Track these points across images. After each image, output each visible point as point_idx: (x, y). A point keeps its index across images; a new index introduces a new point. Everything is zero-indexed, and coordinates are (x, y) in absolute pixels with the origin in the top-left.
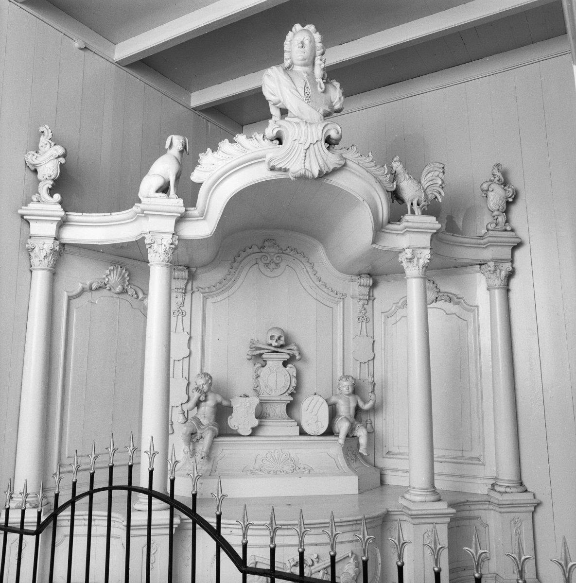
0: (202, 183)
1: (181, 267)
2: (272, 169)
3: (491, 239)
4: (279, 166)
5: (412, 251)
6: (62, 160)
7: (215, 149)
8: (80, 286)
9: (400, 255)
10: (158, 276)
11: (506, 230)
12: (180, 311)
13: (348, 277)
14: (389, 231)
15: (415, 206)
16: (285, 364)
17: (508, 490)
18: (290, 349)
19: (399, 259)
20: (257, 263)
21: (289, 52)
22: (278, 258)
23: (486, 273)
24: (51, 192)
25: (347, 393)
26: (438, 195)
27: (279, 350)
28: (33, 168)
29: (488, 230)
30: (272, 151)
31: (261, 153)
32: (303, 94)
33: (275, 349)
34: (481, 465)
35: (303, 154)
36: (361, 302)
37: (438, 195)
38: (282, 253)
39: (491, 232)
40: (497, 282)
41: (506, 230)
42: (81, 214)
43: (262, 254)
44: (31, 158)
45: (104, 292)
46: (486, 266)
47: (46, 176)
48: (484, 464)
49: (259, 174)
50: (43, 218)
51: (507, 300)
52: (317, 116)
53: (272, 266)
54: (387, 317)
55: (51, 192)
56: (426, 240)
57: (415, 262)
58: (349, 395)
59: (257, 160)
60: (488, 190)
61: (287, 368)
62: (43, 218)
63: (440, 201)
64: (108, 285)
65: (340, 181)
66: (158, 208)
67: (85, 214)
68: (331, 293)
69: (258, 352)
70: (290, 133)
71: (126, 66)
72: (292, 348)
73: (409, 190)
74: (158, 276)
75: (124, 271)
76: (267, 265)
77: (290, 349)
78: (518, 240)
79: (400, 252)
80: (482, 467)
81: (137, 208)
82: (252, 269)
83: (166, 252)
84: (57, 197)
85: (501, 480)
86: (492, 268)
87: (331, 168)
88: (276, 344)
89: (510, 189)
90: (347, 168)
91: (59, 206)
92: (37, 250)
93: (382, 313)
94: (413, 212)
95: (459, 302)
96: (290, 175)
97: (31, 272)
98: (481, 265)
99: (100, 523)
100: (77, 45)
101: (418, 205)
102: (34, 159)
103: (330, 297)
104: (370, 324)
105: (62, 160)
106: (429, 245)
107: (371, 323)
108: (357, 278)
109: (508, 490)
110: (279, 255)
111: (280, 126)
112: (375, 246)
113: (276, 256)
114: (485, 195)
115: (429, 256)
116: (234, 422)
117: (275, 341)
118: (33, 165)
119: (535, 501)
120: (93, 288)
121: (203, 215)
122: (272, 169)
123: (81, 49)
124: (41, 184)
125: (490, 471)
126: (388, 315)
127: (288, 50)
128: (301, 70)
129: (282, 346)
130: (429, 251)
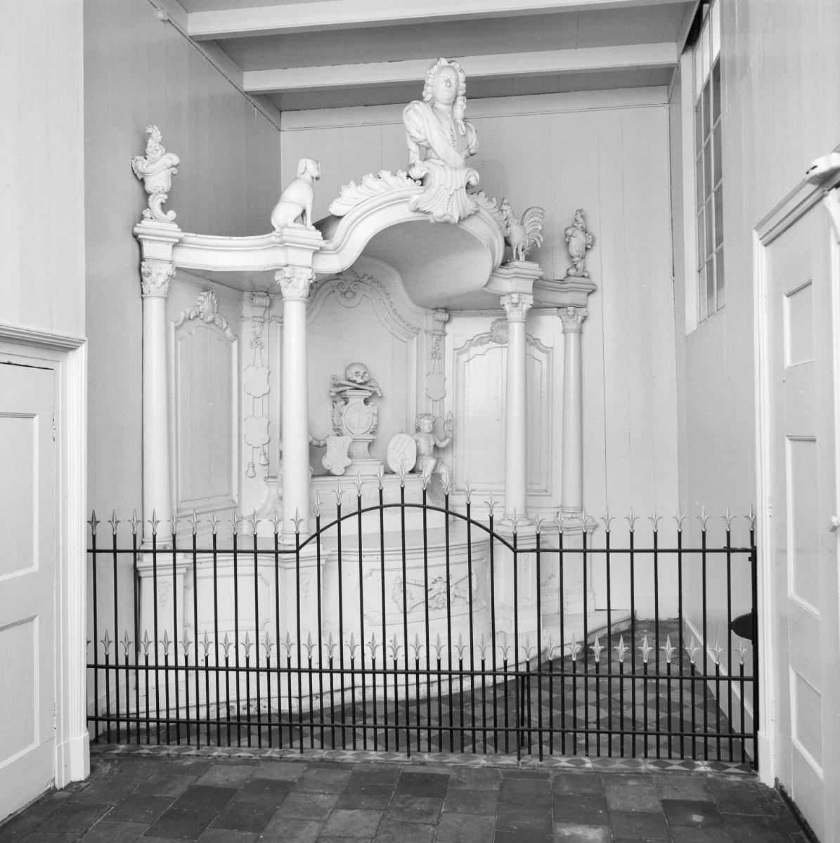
0: (340, 217)
1: (261, 294)
2: (417, 210)
3: (573, 285)
4: (424, 209)
5: (519, 296)
6: (175, 171)
7: (359, 183)
8: (182, 314)
9: (502, 298)
10: (294, 311)
11: (583, 276)
12: (258, 343)
13: (423, 311)
14: (498, 275)
15: (520, 252)
16: (366, 402)
17: (574, 516)
18: (371, 386)
19: (501, 302)
20: (334, 292)
21: (432, 86)
22: (355, 287)
23: (564, 318)
24: (165, 207)
25: (428, 431)
26: (537, 240)
27: (361, 387)
28: (140, 177)
29: (568, 275)
30: (416, 194)
31: (406, 193)
32: (449, 137)
33: (358, 386)
34: (547, 495)
35: (447, 200)
36: (435, 338)
37: (537, 240)
38: (360, 281)
39: (573, 278)
40: (573, 325)
41: (583, 276)
42: (195, 235)
43: (339, 281)
44: (142, 165)
45: (198, 322)
46: (565, 309)
47: (160, 189)
48: (550, 496)
49: (401, 214)
50: (159, 239)
51: (580, 340)
52: (460, 160)
53: (349, 295)
54: (459, 354)
55: (165, 207)
56: (528, 286)
57: (520, 308)
58: (429, 433)
59: (403, 200)
60: (572, 236)
61: (369, 406)
62: (159, 239)
63: (539, 246)
64: (202, 314)
65: (469, 226)
66: (300, 240)
67: (199, 235)
68: (406, 327)
69: (341, 389)
70: (437, 177)
71: (199, 42)
72: (373, 384)
73: (517, 239)
74: (294, 311)
75: (214, 297)
76: (344, 294)
77: (371, 386)
78: (593, 287)
79: (503, 295)
80: (549, 497)
81: (272, 237)
82: (329, 298)
83: (305, 288)
84: (172, 214)
85: (567, 507)
86: (571, 313)
87: (468, 214)
88: (362, 381)
89: (590, 236)
90: (479, 215)
91: (176, 226)
92: (154, 275)
93: (454, 349)
94: (518, 258)
95: (535, 343)
96: (431, 219)
97: (143, 299)
98: (559, 308)
99: (225, 564)
100: (161, 15)
101: (523, 250)
102: (145, 167)
103: (404, 330)
104: (265, 351)
105: (175, 171)
106: (531, 291)
107: (266, 348)
108: (432, 312)
109: (574, 516)
110: (356, 283)
111: (428, 168)
112: (485, 289)
113: (353, 284)
114: (504, 207)
115: (532, 302)
116: (327, 462)
117: (360, 377)
118: (143, 174)
119: (594, 524)
120: (192, 317)
121: (337, 250)
122: (417, 210)
123: (163, 21)
124: (151, 198)
125: (556, 500)
126: (459, 351)
127: (431, 84)
128: (444, 109)
129: (365, 383)
130: (532, 297)
